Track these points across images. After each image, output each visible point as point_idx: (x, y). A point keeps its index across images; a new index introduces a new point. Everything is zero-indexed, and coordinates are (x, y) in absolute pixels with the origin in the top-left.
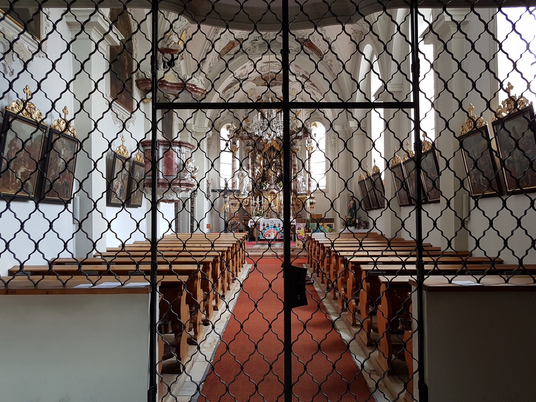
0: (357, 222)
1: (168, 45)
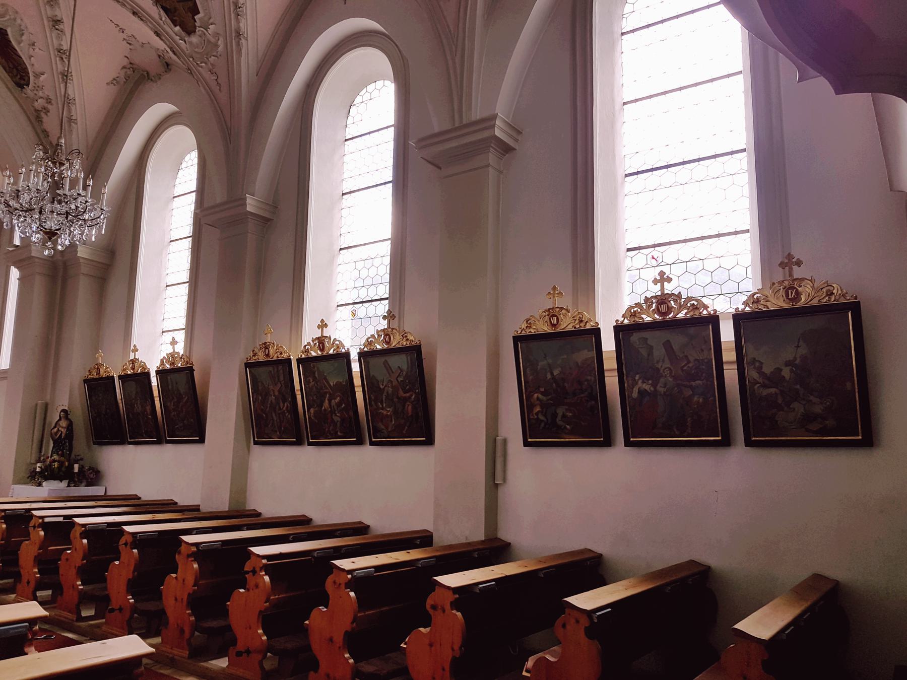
0: (76, 470)
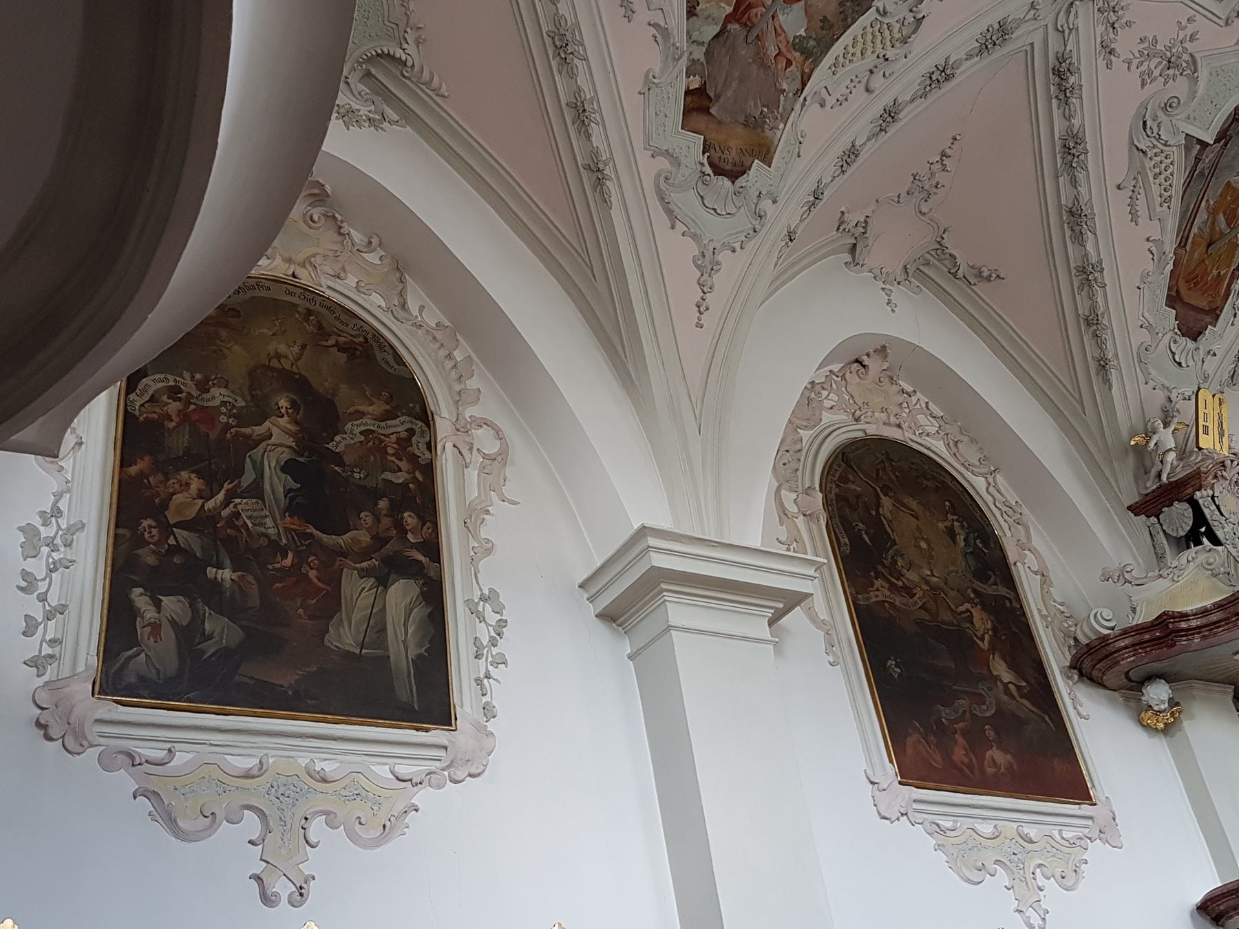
1: (1159, 476)
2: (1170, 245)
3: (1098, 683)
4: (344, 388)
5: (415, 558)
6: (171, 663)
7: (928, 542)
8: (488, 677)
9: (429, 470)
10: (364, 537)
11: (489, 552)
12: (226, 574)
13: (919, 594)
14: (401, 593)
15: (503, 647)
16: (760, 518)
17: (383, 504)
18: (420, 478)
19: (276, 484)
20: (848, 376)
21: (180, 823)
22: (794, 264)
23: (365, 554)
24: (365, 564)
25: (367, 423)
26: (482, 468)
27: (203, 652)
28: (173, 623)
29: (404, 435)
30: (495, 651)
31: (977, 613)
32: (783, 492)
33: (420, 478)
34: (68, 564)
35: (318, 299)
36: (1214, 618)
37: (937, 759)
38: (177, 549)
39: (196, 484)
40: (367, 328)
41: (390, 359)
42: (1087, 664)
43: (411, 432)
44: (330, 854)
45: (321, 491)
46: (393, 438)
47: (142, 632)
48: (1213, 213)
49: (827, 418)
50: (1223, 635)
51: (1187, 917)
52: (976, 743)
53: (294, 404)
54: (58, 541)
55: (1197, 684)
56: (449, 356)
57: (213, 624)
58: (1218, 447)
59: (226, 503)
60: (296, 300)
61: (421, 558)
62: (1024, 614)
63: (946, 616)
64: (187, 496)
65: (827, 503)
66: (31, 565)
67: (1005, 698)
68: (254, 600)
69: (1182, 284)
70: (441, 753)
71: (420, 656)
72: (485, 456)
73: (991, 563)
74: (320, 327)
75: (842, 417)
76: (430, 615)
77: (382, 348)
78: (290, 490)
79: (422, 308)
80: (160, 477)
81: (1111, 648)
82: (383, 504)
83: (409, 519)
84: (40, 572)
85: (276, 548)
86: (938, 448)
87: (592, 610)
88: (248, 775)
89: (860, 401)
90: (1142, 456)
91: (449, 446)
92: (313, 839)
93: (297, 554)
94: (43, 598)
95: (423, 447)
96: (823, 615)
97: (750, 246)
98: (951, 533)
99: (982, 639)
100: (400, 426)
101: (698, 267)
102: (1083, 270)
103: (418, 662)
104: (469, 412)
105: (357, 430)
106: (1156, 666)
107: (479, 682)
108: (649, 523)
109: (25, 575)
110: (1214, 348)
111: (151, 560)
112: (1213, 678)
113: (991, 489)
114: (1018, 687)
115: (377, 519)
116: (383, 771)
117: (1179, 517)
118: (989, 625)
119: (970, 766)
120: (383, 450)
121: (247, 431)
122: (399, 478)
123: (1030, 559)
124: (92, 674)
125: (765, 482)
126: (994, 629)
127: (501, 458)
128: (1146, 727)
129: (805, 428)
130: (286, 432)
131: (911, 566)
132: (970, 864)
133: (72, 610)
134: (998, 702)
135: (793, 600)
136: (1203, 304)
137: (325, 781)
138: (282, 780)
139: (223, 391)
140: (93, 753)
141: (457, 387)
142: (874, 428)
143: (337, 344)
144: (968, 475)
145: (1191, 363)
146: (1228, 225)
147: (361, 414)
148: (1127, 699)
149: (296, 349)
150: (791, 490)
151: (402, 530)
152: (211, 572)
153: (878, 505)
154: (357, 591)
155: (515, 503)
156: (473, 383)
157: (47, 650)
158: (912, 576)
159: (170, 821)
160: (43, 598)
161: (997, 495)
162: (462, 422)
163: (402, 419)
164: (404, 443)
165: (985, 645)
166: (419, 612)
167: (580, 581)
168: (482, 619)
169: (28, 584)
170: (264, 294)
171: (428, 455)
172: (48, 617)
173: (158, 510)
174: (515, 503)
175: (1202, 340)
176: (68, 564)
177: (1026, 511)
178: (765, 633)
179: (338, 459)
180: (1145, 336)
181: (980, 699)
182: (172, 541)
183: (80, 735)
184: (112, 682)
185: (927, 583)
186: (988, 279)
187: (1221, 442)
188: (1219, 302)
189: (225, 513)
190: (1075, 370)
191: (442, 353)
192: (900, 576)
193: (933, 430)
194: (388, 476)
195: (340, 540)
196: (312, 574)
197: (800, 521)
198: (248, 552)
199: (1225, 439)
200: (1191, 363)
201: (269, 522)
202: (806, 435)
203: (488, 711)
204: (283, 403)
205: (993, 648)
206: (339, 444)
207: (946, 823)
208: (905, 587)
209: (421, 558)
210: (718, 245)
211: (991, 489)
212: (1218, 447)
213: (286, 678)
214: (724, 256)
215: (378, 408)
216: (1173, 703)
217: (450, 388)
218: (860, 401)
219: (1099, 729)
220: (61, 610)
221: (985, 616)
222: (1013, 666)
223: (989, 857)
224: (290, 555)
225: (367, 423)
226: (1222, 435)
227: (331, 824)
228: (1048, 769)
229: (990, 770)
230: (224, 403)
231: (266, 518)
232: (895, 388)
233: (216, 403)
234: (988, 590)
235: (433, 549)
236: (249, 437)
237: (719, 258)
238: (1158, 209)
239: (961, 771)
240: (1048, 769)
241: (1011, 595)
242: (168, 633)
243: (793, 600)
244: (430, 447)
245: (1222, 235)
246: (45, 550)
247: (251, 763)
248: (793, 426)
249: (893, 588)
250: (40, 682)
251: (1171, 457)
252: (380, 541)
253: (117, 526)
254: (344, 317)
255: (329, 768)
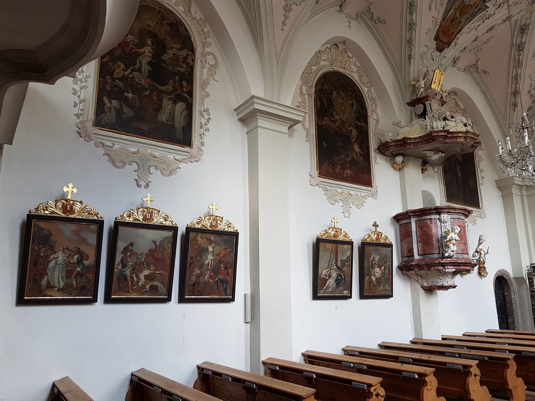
2: (439, 20)
3: (383, 154)
4: (168, 38)
5: (185, 97)
6: (114, 121)
7: (345, 107)
8: (203, 134)
9: (191, 69)
10: (171, 88)
11: (208, 96)
12: (130, 95)
13: (338, 123)
14: (180, 107)
15: (209, 126)
16: (293, 95)
17: (177, 78)
18: (189, 70)
19: (146, 68)
20: (332, 49)
21: (116, 164)
22: (318, 10)
23: (170, 93)
24: (170, 96)
25: (174, 51)
26: (209, 69)
27: (123, 117)
28: (115, 108)
29: (185, 56)
30: (206, 127)
31: (354, 131)
32: (303, 87)
33: (189, 70)
34: (86, 87)
35: (163, 7)
36: (418, 141)
37: (331, 172)
38: (116, 86)
39: (122, 66)
40: (177, 18)
41: (184, 30)
42: (381, 149)
43: (188, 55)
44: (155, 176)
45: (159, 71)
46: (182, 56)
47: (106, 110)
48: (456, 10)
49: (322, 63)
50: (419, 145)
51: (390, 219)
52: (343, 167)
53: (152, 43)
54: (83, 80)
55: (411, 158)
56: (202, 30)
57: (126, 110)
58: (437, 88)
59: (131, 73)
60: (155, 7)
61: (187, 96)
62: (368, 132)
63: (344, 130)
64: (120, 70)
65: (316, 92)
66: (75, 87)
67: (355, 156)
68: (137, 104)
69: (440, 33)
70: (188, 154)
71: (184, 126)
72: (210, 65)
73: (362, 116)
74: (163, 17)
75: (327, 63)
76: (188, 114)
77: (181, 26)
78: (150, 71)
79: (196, 12)
80: (112, 63)
81: (388, 145)
82: (177, 78)
83: (184, 83)
84: (78, 89)
85: (144, 89)
86: (355, 77)
87: (237, 118)
88: (134, 153)
89: (334, 58)
90: (415, 88)
91: (199, 61)
92: (151, 172)
93: (150, 91)
94: (79, 97)
95: (191, 60)
96: (307, 126)
97: (303, 4)
98: (352, 105)
99: (353, 138)
100: (184, 53)
101: (285, 10)
102: (410, 25)
103: (183, 127)
104: (207, 50)
105: (171, 53)
106: (401, 152)
107: (200, 135)
108: (255, 94)
109: (74, 89)
110: (446, 55)
111: (109, 89)
112: (416, 157)
113: (369, 92)
114: (360, 153)
115: (175, 82)
116: (171, 157)
117: (420, 108)
118: (356, 134)
119: (340, 174)
120: (178, 60)
121: (138, 50)
122: (182, 70)
123: (375, 116)
124: (92, 120)
125: (297, 81)
126: (358, 136)
127: (214, 67)
128: (394, 168)
129: (314, 66)
130: (149, 52)
131: (337, 114)
132: (332, 199)
133: (87, 101)
134: (353, 157)
135: (296, 122)
136: (445, 40)
137: (155, 157)
138: (143, 156)
139: (132, 37)
140: (93, 142)
141: (204, 41)
142: (336, 68)
143: (167, 23)
144: (363, 86)
145: (437, 60)
146: (460, 15)
147: (173, 48)
148: (391, 159)
149: (155, 24)
150: (306, 86)
151: (182, 87)
152: (126, 94)
153: (332, 93)
154: (167, 104)
155: (217, 81)
156: (209, 40)
157: (80, 112)
158: (337, 117)
159: (113, 162)
160: (79, 97)
161: (370, 94)
162: (204, 53)
163: (185, 50)
164: (185, 58)
165: (353, 140)
166: (185, 113)
167: (236, 106)
168: (203, 117)
169: (75, 92)
170: (146, 4)
171: (192, 63)
172: (80, 102)
173: (111, 74)
174: (217, 81)
175: (443, 52)
176: (86, 87)
177: (377, 100)
178: (286, 130)
179: (164, 62)
180: (425, 49)
181: (348, 156)
182: (115, 83)
183: (89, 137)
184: (98, 123)
185: (341, 120)
186: (382, 22)
187: (438, 87)
188: (451, 41)
189: (130, 76)
190: (401, 58)
191: (200, 29)
192: (333, 117)
193: (355, 71)
194: (179, 69)
195: (164, 88)
196: (154, 98)
197: (306, 97)
198: (136, 89)
199: (440, 86)
200: (437, 60)
201: (143, 80)
202: (314, 68)
203: (202, 144)
204: (149, 42)
205: (356, 141)
206: (165, 57)
207: (329, 188)
208: (334, 120)
209: (187, 96)
210: (292, 3)
211: (369, 92)
212: (437, 88)
213: (145, 128)
214: (294, 7)
215: (178, 46)
216: (403, 162)
217: (201, 40)
218: (334, 58)
219: (381, 168)
220: (84, 101)
221: (356, 131)
222: (360, 147)
223: (338, 198)
224: (148, 91)
225: (174, 51)
226: (439, 85)
227: (156, 169)
228: (362, 176)
229: (345, 175)
230: (131, 41)
231: (142, 80)
232: (346, 55)
233: (129, 40)
234: (359, 124)
235: (191, 94)
236: (138, 52)
237: (292, 7)
238: (438, 7)
239: (337, 175)
240: (362, 176)
241: (365, 126)
242: (113, 111)
243: (296, 122)
244: (193, 60)
245: (457, 18)
246: (79, 82)
247: (135, 150)
248: (310, 64)
249: (330, 120)
250: (78, 121)
251: (422, 90)
252: (175, 89)
253: (100, 77)
254: (170, 14)
255: (156, 154)
